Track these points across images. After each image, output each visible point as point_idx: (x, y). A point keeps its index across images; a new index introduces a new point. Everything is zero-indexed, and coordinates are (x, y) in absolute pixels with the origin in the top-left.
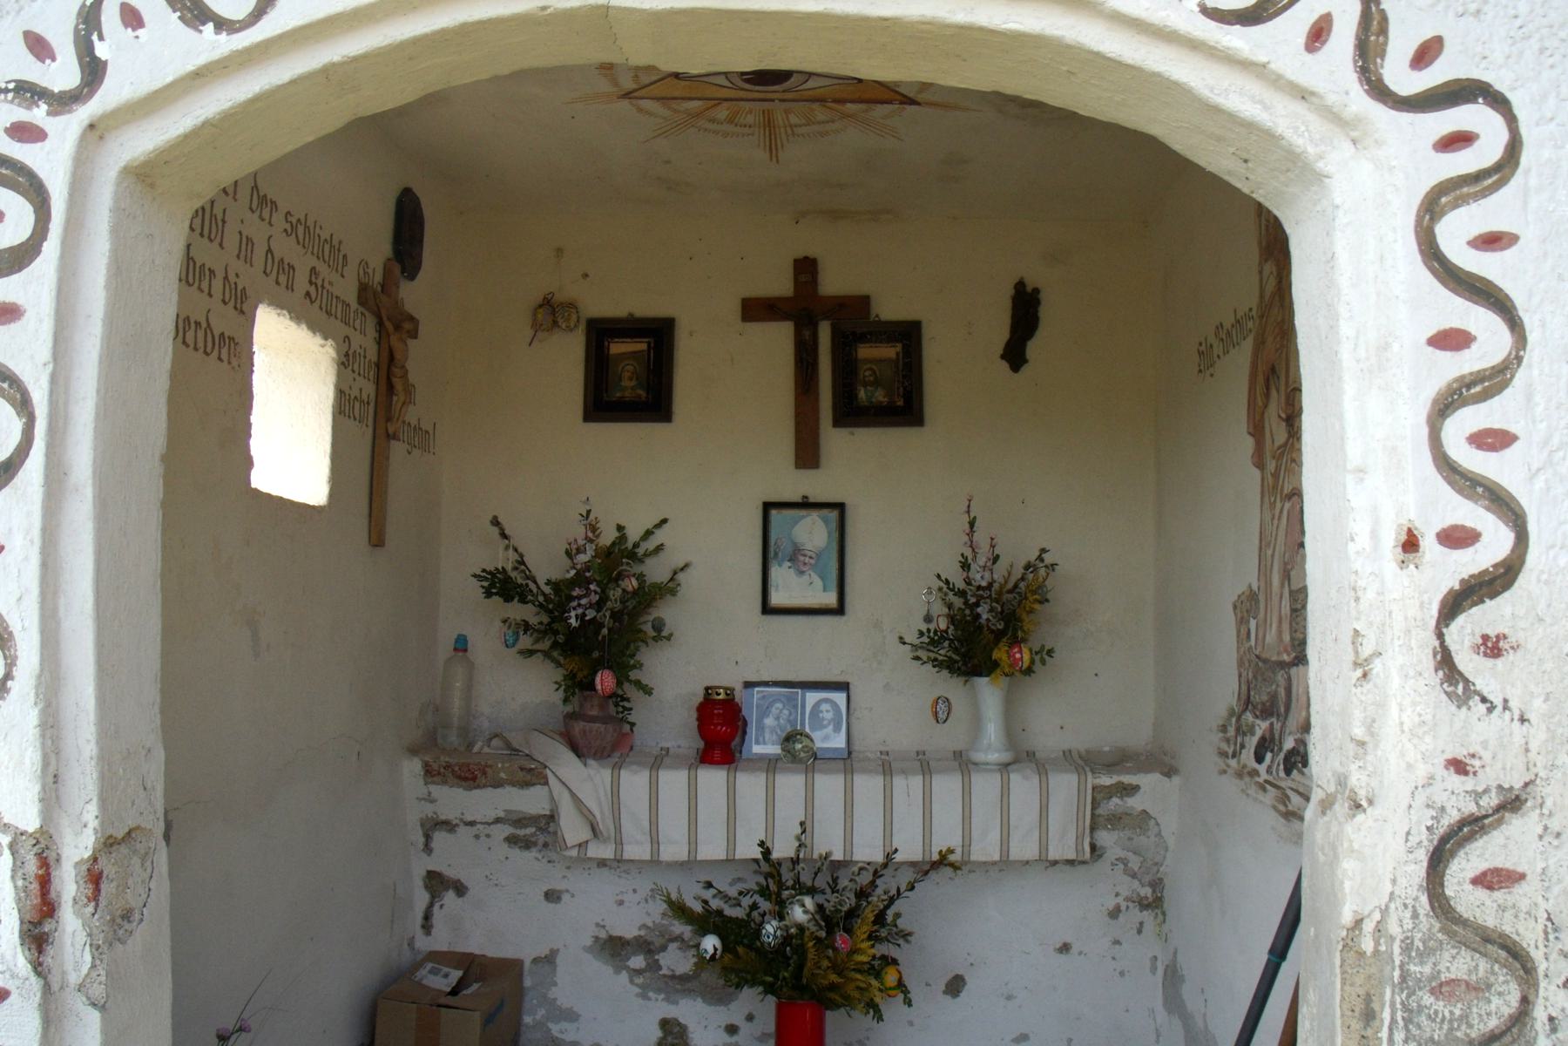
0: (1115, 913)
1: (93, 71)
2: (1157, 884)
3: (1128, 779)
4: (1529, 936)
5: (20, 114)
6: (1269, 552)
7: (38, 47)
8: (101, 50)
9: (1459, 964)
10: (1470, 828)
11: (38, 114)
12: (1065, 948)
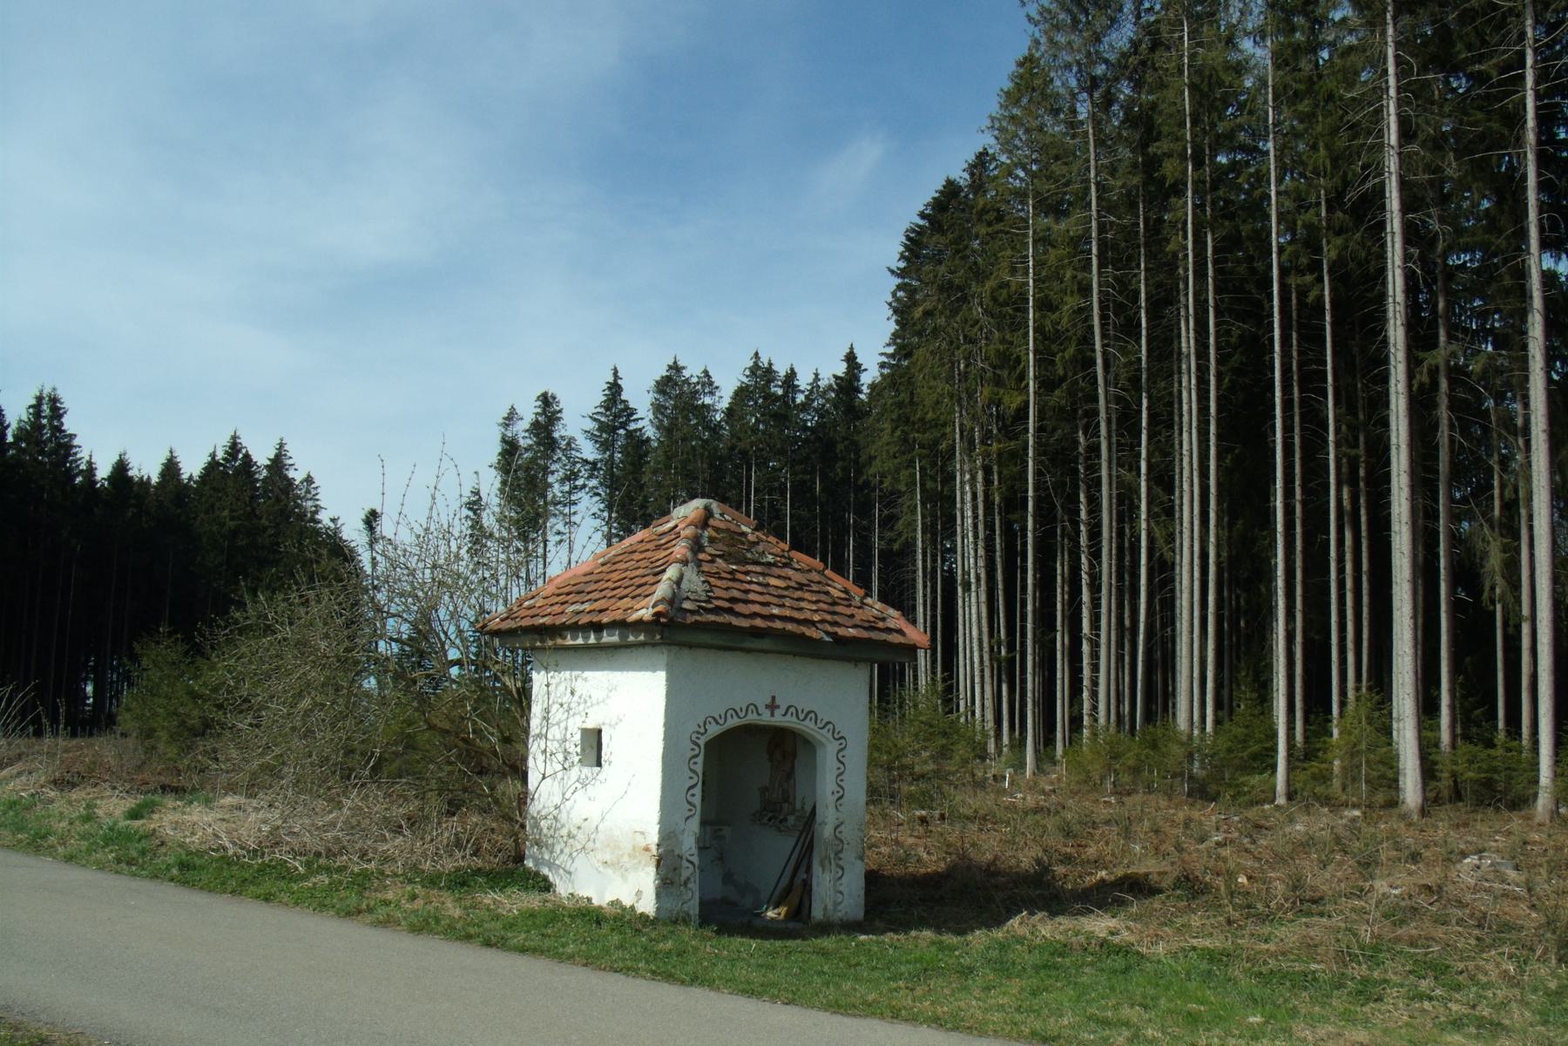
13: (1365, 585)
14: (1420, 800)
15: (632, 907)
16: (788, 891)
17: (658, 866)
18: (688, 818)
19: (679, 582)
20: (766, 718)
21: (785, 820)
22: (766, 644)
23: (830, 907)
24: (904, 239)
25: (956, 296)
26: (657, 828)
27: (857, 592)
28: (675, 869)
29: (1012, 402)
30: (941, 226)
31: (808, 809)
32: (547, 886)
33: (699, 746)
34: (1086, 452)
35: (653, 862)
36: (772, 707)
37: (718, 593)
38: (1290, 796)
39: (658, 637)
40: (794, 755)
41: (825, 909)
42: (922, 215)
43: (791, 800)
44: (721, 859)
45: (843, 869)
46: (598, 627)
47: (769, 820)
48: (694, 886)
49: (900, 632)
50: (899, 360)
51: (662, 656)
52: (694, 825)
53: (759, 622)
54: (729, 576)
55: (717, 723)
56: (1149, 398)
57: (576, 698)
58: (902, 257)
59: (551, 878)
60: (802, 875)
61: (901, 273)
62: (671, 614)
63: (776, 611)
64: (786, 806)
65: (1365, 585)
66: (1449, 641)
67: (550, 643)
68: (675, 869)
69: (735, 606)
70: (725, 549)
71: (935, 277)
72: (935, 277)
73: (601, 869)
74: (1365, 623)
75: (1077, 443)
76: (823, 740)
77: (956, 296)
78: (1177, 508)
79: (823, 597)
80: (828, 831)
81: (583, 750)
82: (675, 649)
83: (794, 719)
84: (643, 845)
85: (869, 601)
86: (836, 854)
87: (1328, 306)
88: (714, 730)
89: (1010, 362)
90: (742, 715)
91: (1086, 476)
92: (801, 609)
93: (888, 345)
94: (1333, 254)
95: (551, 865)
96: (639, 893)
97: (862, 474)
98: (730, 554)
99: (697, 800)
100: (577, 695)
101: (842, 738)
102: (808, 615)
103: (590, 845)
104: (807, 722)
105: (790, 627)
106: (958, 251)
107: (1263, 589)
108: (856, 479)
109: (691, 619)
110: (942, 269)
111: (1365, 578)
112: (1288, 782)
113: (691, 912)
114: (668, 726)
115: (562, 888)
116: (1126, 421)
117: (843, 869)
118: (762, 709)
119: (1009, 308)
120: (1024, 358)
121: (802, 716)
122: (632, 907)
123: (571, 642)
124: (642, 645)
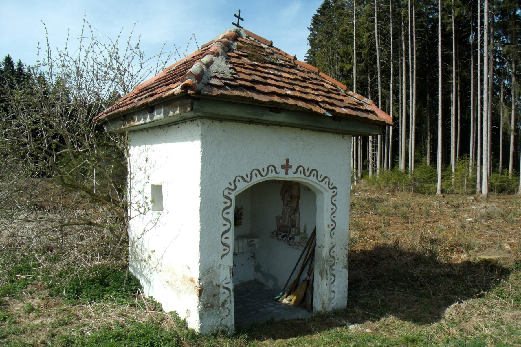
0: (248, 259)
1: (236, 187)
2: (254, 254)
3: (253, 239)
4: (335, 256)
5: (229, 191)
6: (285, 213)
7: (230, 184)
8: (236, 184)
9: (331, 259)
10: (332, 248)
11: (230, 191)
12: (242, 265)
14: (487, 192)
16: (296, 284)
18: (223, 256)
19: (208, 65)
20: (282, 176)
21: (292, 238)
22: (281, 118)
23: (326, 302)
24: (312, 18)
25: (329, 35)
27: (342, 87)
28: (214, 295)
29: (348, 67)
30: (324, 14)
31: (309, 233)
33: (230, 199)
34: (371, 83)
36: (287, 167)
37: (242, 76)
38: (442, 191)
39: (189, 109)
40: (299, 198)
41: (323, 303)
42: (318, 11)
43: (296, 226)
44: (253, 257)
45: (334, 276)
47: (283, 237)
49: (373, 112)
50: (310, 58)
51: (197, 128)
52: (229, 260)
53: (276, 99)
54: (252, 68)
55: (245, 181)
56: (393, 64)
58: (312, 24)
60: (305, 276)
61: (311, 30)
62: (198, 87)
63: (289, 92)
64: (293, 229)
66: (490, 141)
68: (214, 295)
69: (255, 86)
70: (250, 52)
71: (323, 29)
72: (323, 29)
75: (368, 80)
77: (329, 35)
78: (400, 100)
79: (321, 88)
80: (325, 252)
82: (207, 122)
83: (302, 175)
84: (189, 277)
85: (350, 92)
86: (331, 267)
87: (453, 32)
88: (242, 186)
89: (347, 56)
90: (264, 174)
91: (371, 91)
92: (306, 93)
93: (307, 54)
94: (456, 14)
95: (141, 274)
98: (253, 56)
99: (230, 242)
100: (149, 161)
102: (312, 97)
104: (311, 177)
105: (300, 104)
106: (329, 21)
107: (424, 126)
109: (216, 92)
110: (325, 27)
111: (459, 122)
112: (441, 186)
113: (228, 325)
114: (203, 184)
116: (385, 72)
117: (334, 276)
118: (279, 169)
119: (346, 40)
120: (351, 53)
121: (307, 174)
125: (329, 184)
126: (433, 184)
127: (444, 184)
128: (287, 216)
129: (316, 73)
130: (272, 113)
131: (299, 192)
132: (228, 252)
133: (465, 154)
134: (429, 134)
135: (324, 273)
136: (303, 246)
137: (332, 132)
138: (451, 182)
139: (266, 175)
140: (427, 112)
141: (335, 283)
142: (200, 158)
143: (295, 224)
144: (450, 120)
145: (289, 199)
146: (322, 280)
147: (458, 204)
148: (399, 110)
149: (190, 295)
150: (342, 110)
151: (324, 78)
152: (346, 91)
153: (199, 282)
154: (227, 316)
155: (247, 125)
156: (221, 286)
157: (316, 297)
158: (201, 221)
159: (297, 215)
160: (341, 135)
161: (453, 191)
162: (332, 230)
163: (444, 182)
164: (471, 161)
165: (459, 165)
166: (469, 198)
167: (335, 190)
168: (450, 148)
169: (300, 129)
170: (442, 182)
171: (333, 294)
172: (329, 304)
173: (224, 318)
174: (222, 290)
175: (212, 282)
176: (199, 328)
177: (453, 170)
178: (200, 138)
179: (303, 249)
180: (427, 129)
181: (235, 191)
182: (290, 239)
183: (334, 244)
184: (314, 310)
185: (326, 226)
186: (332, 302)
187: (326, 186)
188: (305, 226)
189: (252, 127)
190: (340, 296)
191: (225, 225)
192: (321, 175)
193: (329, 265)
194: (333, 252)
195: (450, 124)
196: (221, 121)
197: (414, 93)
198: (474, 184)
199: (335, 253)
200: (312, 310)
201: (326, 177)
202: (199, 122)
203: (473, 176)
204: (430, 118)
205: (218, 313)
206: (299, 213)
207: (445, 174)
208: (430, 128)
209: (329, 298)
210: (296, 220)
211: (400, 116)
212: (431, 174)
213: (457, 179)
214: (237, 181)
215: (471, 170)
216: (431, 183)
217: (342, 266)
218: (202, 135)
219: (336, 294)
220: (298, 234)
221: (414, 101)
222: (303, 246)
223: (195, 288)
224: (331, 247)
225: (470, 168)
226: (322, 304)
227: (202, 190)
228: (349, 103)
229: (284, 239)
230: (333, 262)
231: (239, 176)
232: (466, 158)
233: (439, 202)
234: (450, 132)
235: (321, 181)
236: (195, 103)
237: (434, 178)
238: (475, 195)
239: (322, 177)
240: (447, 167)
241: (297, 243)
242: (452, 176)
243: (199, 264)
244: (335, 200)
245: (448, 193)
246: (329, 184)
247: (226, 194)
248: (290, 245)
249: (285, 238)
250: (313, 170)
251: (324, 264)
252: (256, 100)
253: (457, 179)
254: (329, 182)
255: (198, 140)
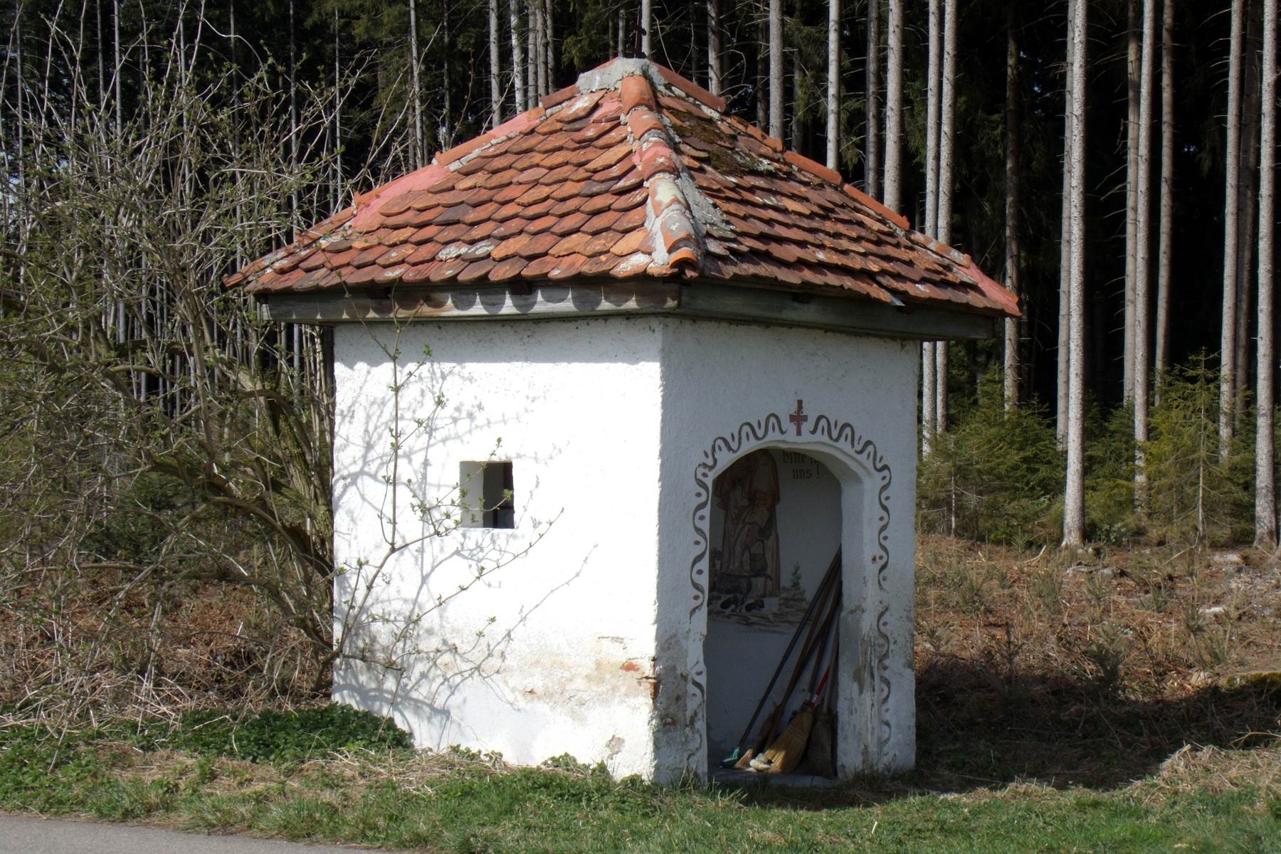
1: (715, 461)
4: (889, 635)
9: (881, 641)
13: (1165, 201)
15: (602, 768)
17: (655, 695)
22: (809, 313)
23: (873, 749)
26: (652, 630)
31: (810, 586)
32: (401, 741)
35: (647, 688)
36: (798, 418)
38: (1088, 532)
40: (776, 498)
41: (865, 752)
43: (769, 572)
45: (888, 684)
46: (483, 286)
48: (701, 725)
49: (974, 287)
51: (655, 336)
55: (730, 449)
57: (448, 411)
59: (400, 724)
64: (759, 582)
65: (1165, 201)
67: (403, 314)
68: (678, 698)
73: (522, 703)
74: (1164, 260)
76: (860, 471)
78: (872, 78)
80: (867, 622)
81: (464, 494)
83: (825, 438)
84: (622, 658)
85: (918, 236)
86: (880, 661)
88: (726, 459)
96: (615, 744)
97: (310, 10)
101: (885, 467)
103: (495, 662)
107: (987, 208)
108: (299, 21)
109: (729, 271)
111: (1165, 189)
112: (1083, 510)
115: (425, 736)
117: (888, 684)
121: (835, 434)
122: (602, 768)
123: (456, 312)
124: (629, 315)
125: (875, 459)
126: (1044, 500)
127: (1098, 499)
128: (738, 549)
129: (836, 188)
130: (796, 304)
131: (777, 484)
132: (702, 604)
133: (1197, 352)
134: (1012, 247)
135: (867, 675)
136: (790, 622)
137: (881, 337)
138: (1131, 492)
139: (764, 436)
140: (1004, 135)
141: (891, 700)
142: (660, 400)
143: (765, 568)
144: (1123, 176)
145: (745, 503)
146: (861, 692)
147: (1171, 578)
148: (863, 130)
149: (622, 701)
150: (918, 289)
151: (855, 200)
152: (908, 233)
153: (654, 666)
154: (697, 749)
155: (733, 327)
156: (690, 677)
157: (846, 738)
158: (660, 533)
159: (770, 542)
160: (899, 341)
161: (1140, 532)
162: (881, 570)
163: (1094, 489)
164: (1225, 388)
165: (1169, 408)
166: (1217, 558)
167: (886, 473)
168: (1121, 320)
169: (822, 332)
170: (1084, 489)
171: (886, 728)
172: (880, 753)
173: (693, 754)
174: (692, 689)
175: (674, 668)
176: (653, 770)
177: (1140, 433)
178: (658, 358)
179: (794, 630)
180: (1004, 225)
181: (714, 470)
182: (749, 608)
183: (885, 604)
184: (840, 775)
185: (867, 557)
186: (885, 749)
187: (869, 464)
188: (797, 569)
189: (741, 331)
190: (900, 736)
191: (697, 543)
192: (860, 438)
193: (877, 654)
194: (885, 624)
195: (1121, 200)
196: (694, 321)
197: (949, 47)
198: (1241, 495)
199: (888, 626)
200: (836, 774)
201: (868, 443)
202: (655, 323)
203: (1237, 458)
204: (1018, 169)
205: (683, 739)
206: (777, 538)
207: (1097, 452)
208: (1019, 216)
209: (879, 738)
210: (768, 555)
211: (871, 161)
212: (1029, 453)
213: (1161, 474)
214: (717, 449)
215: (1225, 432)
216: (1031, 493)
217: (903, 661)
218: (663, 350)
219: (893, 729)
220: (776, 590)
221: (947, 88)
222: (790, 622)
223: (640, 683)
224: (881, 610)
225: (1223, 419)
226: (863, 754)
227: (662, 466)
228: (927, 270)
229: (728, 611)
230: (885, 648)
231: (720, 438)
232: (1201, 371)
233: (1085, 569)
234: (1123, 243)
235: (860, 452)
236: (685, 291)
237: (1044, 471)
238: (1247, 551)
239: (862, 442)
240: (1105, 415)
241: (771, 617)
242: (1133, 458)
243: (655, 626)
244: (887, 498)
245: (1118, 543)
246: (875, 459)
247: (700, 476)
248: (749, 624)
249: (733, 607)
250: (846, 425)
251: (866, 653)
252: (782, 281)
253: (1161, 474)
254: (875, 452)
255: (654, 360)
